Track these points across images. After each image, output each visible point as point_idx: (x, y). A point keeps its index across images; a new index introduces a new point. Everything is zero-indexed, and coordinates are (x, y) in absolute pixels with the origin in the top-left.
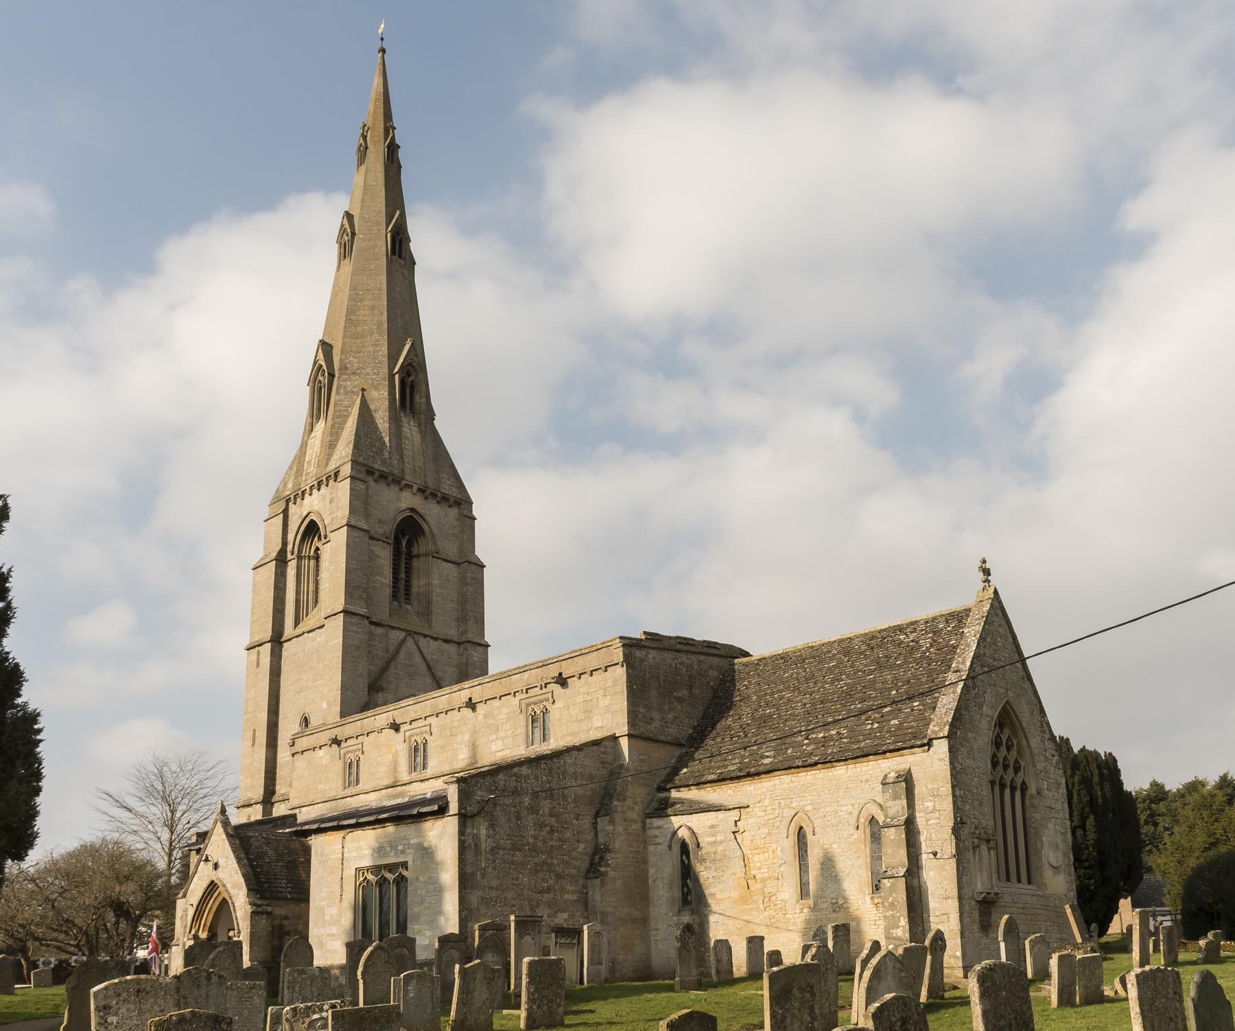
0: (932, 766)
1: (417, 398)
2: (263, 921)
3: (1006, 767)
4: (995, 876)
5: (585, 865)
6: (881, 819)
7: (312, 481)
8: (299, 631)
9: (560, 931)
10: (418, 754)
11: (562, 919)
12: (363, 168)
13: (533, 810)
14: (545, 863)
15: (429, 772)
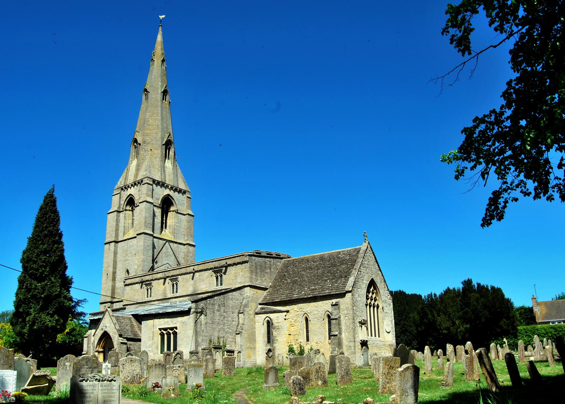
3: (371, 300)
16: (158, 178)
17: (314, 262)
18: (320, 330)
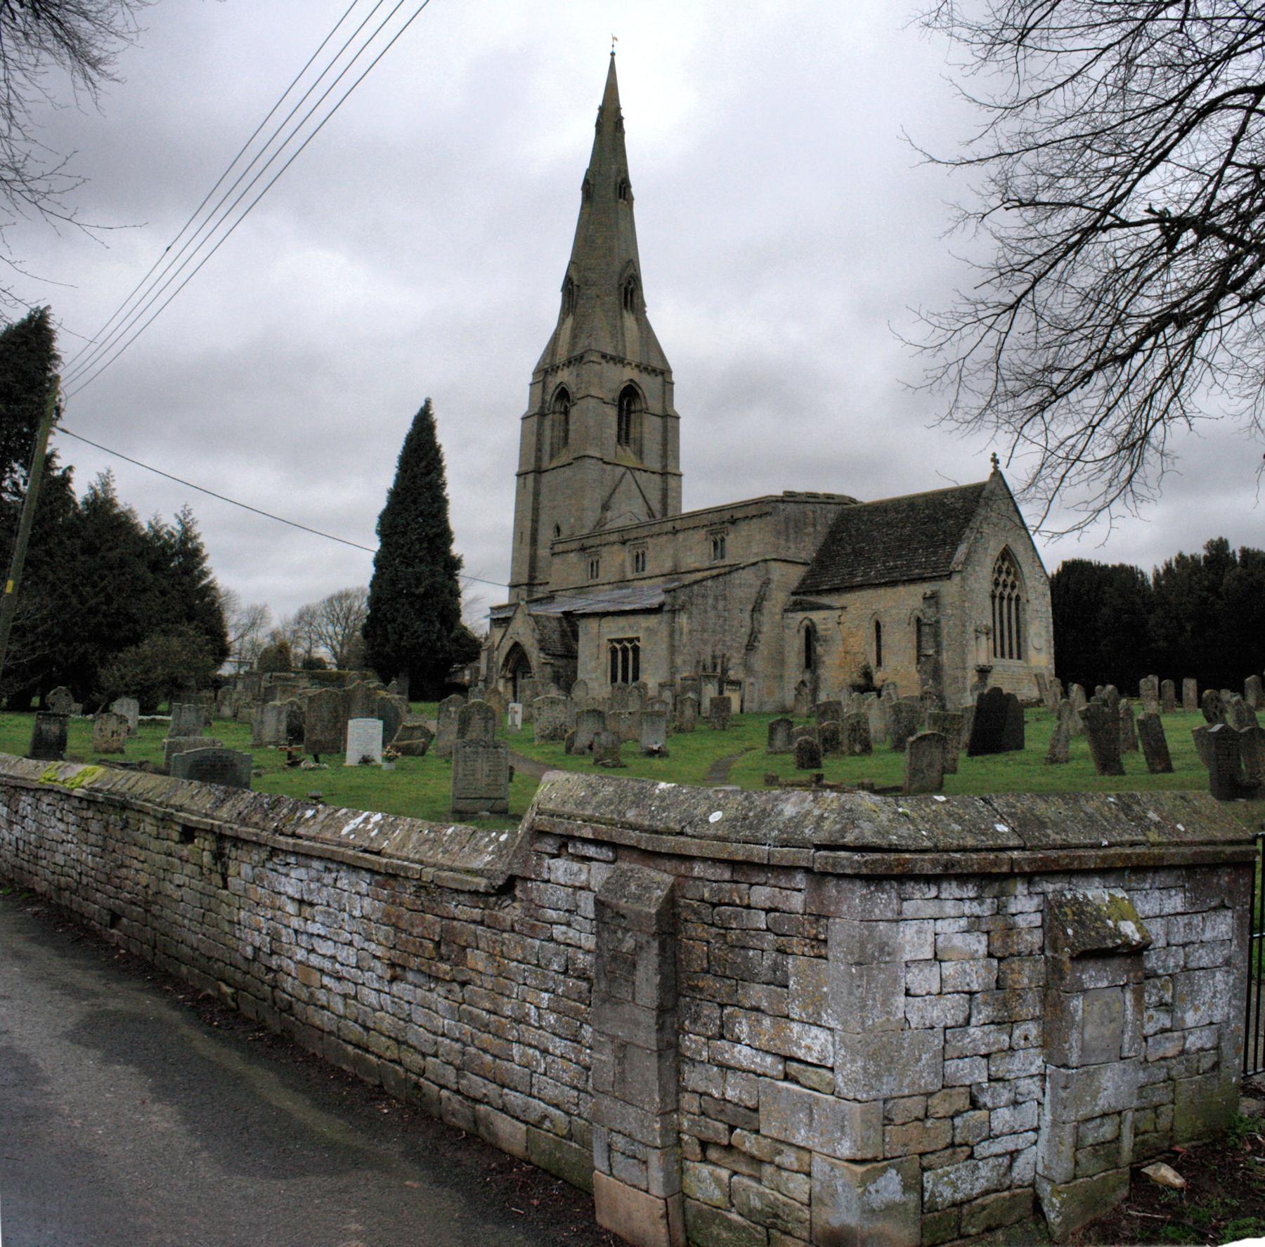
3: (1005, 586)
5: (745, 642)
13: (714, 607)
16: (610, 351)
17: (897, 512)
18: (900, 643)
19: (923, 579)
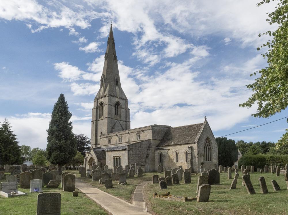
0: (195, 146)
1: (118, 83)
2: (99, 163)
3: (207, 145)
4: (204, 160)
5: (145, 157)
6: (188, 152)
7: (101, 96)
8: (100, 119)
9: (142, 165)
10: (120, 139)
11: (142, 164)
12: (108, 45)
14: (140, 156)
15: (122, 142)
19: (188, 144)
